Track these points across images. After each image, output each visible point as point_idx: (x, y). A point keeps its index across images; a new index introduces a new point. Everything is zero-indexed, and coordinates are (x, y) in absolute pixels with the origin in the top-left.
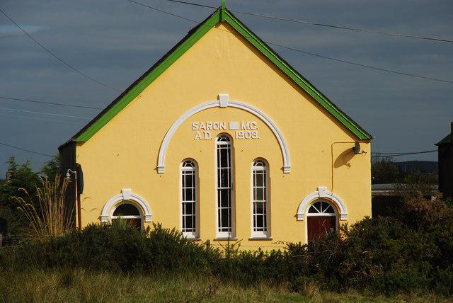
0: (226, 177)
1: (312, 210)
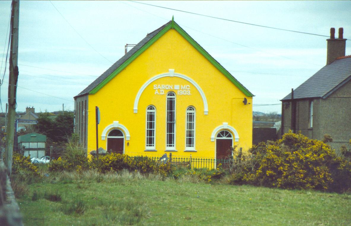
0: (171, 117)
1: (219, 136)
